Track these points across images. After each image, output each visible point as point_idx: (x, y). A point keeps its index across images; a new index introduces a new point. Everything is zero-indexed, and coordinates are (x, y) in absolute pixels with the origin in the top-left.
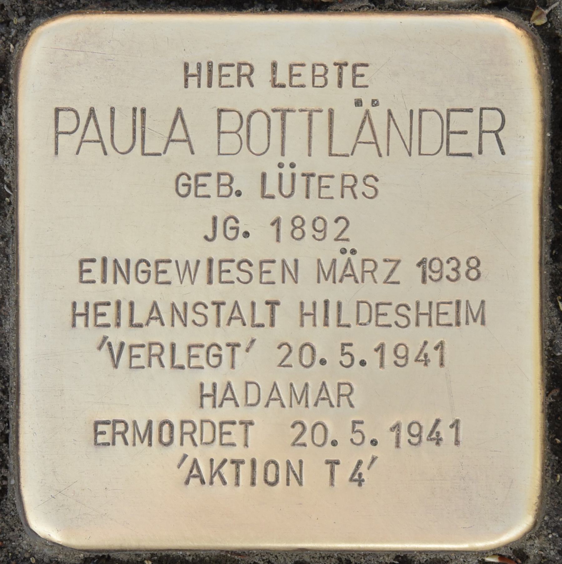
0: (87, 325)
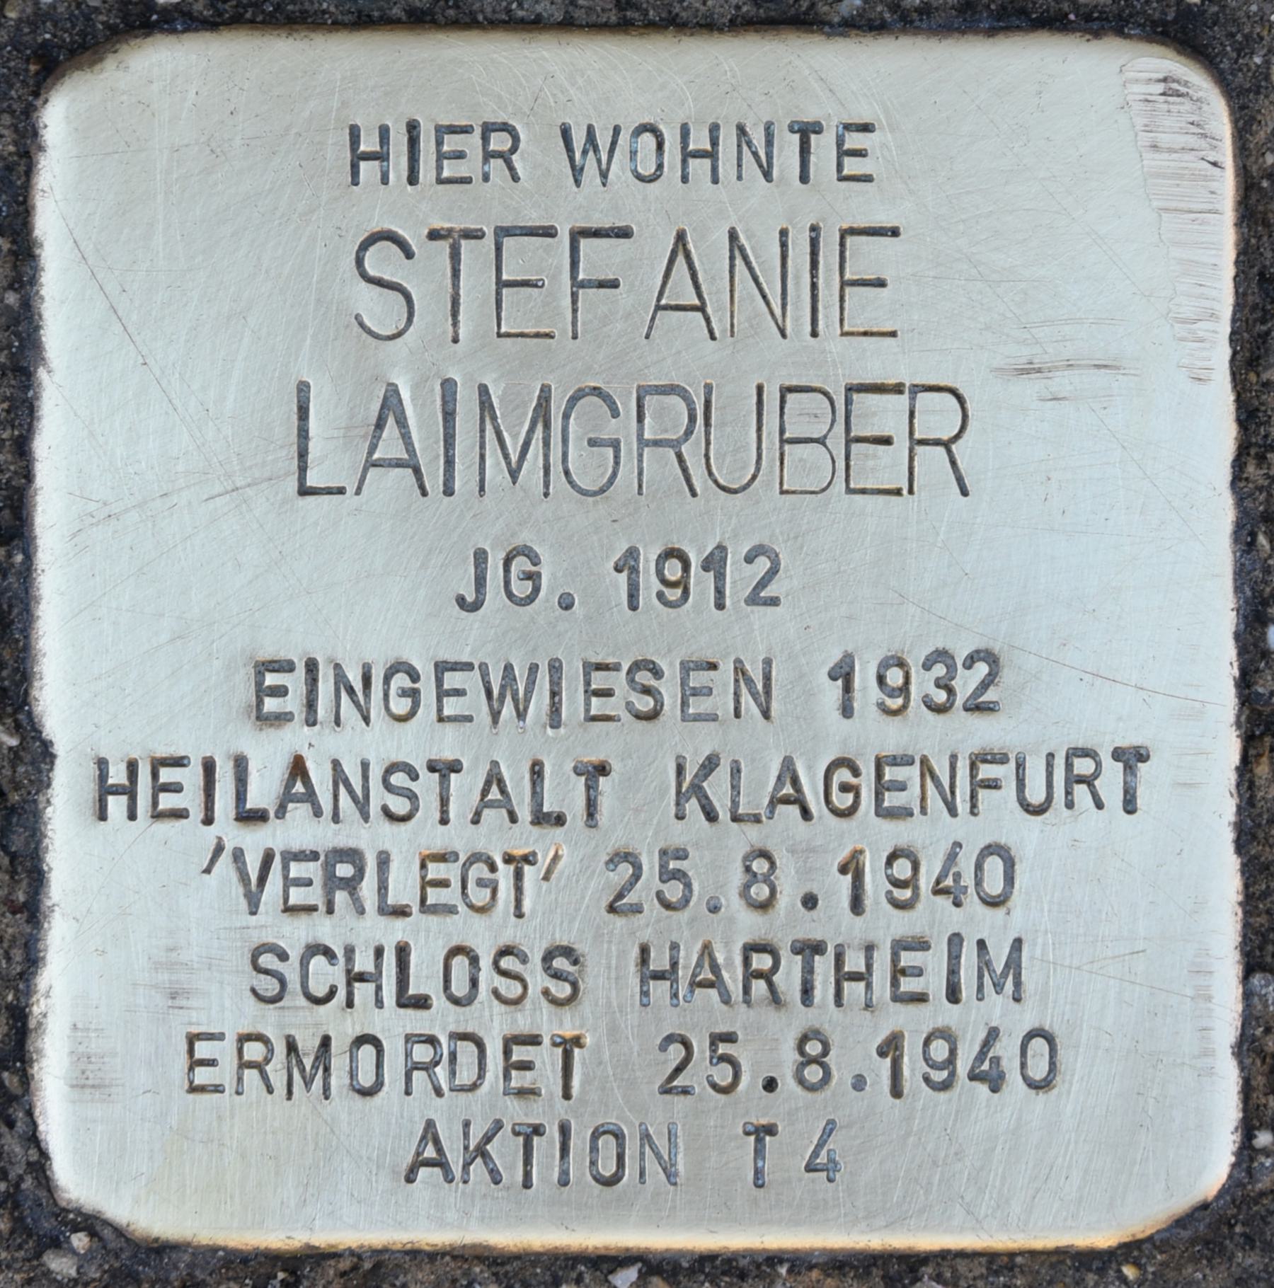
0: (132, 816)
